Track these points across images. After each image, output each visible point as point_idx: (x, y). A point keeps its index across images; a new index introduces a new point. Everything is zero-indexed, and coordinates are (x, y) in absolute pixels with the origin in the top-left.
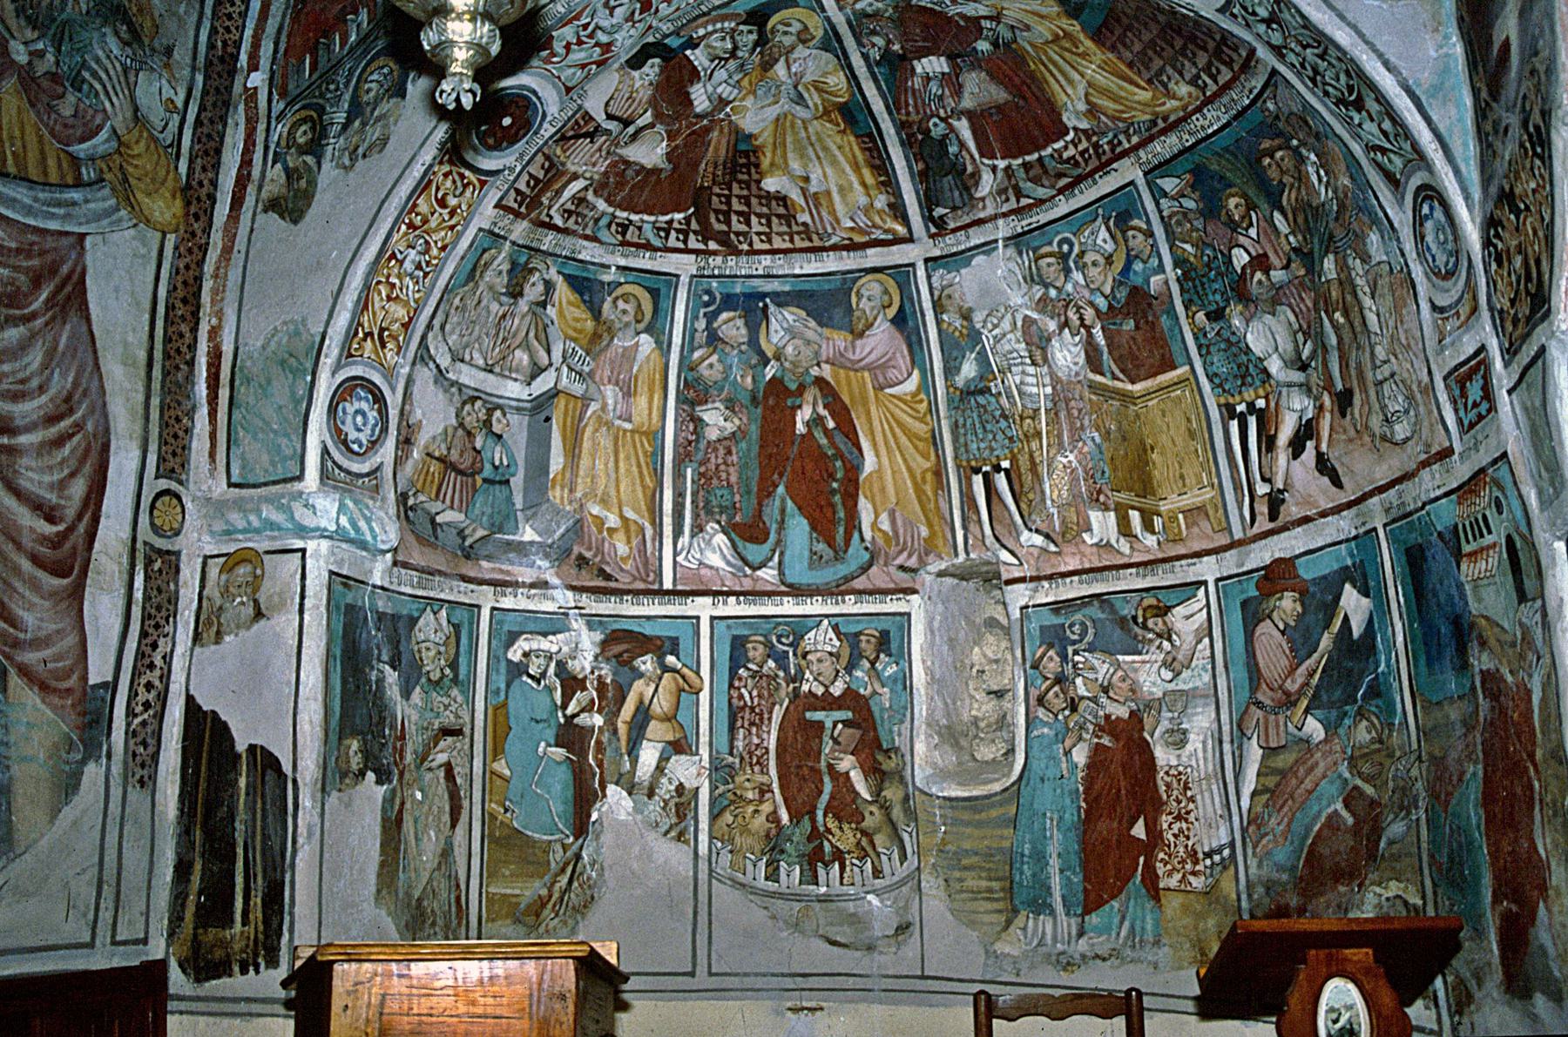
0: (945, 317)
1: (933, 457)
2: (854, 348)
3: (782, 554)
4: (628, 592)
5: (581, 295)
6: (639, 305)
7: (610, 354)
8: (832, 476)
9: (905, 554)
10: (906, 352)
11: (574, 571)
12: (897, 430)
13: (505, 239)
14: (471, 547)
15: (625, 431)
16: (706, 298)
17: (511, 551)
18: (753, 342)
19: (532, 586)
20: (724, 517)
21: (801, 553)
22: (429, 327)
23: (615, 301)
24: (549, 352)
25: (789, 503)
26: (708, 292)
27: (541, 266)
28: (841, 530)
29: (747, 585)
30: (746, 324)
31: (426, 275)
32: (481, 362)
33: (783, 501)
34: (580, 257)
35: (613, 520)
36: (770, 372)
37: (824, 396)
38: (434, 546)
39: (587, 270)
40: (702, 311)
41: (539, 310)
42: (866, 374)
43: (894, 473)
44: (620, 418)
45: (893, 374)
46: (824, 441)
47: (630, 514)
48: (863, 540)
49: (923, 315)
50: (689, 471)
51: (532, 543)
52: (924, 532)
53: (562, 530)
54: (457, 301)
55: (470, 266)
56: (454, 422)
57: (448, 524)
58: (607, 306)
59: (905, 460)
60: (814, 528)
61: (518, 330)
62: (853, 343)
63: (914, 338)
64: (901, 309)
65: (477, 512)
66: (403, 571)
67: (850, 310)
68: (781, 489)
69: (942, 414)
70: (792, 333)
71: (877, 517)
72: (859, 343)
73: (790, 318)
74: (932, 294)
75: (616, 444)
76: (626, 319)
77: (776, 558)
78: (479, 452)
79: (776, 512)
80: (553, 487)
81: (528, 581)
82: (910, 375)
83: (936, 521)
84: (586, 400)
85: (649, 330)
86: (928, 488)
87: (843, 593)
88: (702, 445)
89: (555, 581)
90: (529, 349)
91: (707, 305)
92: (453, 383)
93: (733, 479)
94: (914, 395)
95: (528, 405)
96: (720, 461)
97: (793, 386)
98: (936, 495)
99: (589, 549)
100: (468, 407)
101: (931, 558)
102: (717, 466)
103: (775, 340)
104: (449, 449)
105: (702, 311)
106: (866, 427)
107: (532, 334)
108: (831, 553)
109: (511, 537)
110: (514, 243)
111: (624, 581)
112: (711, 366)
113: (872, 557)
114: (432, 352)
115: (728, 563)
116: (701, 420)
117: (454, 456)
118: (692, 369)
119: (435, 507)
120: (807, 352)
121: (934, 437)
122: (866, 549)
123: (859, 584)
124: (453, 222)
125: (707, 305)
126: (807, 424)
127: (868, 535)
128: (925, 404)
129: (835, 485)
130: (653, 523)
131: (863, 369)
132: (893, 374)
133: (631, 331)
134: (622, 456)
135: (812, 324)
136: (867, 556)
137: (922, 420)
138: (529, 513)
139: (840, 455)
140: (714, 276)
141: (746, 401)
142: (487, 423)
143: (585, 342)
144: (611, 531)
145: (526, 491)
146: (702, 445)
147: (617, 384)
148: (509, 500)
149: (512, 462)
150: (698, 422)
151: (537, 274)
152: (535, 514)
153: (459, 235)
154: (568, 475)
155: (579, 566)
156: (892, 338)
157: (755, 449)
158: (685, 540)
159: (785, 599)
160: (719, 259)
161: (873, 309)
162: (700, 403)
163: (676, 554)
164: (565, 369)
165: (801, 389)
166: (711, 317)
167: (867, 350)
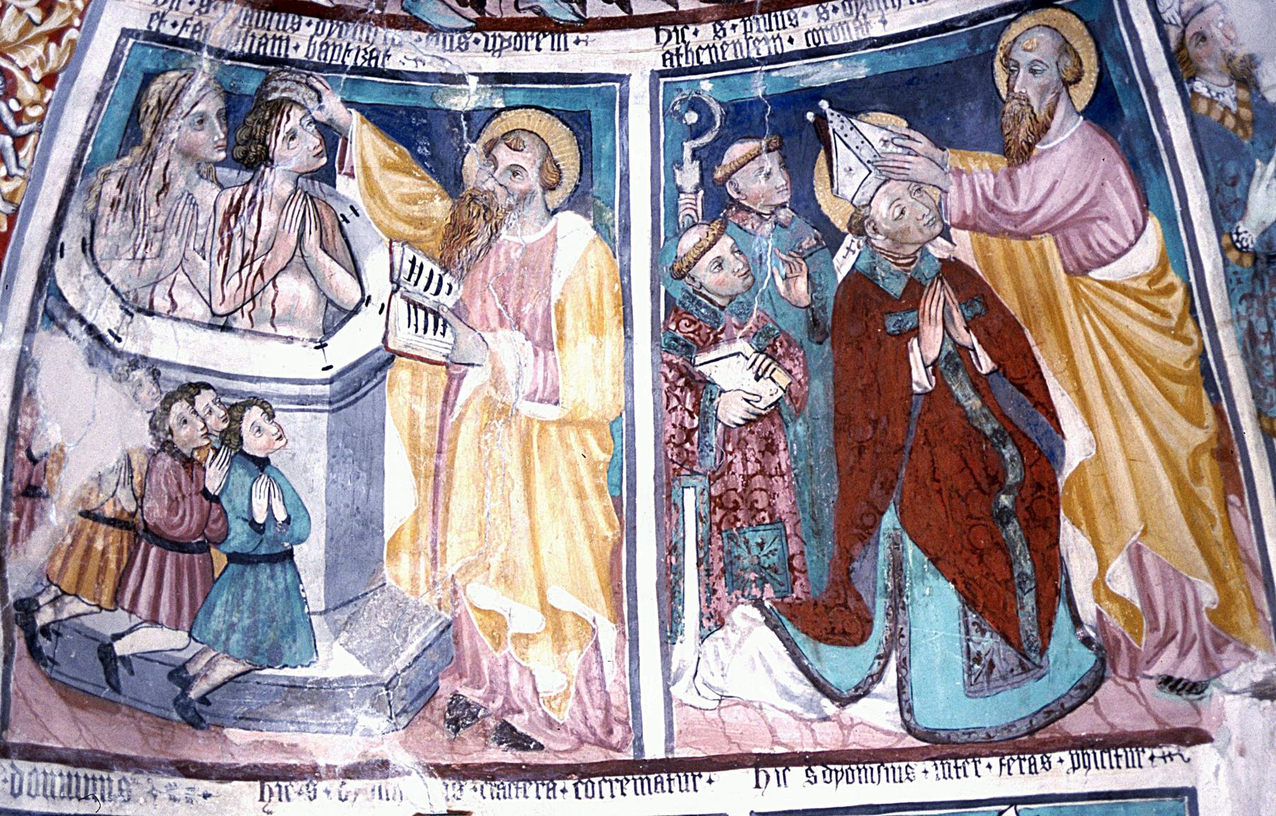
0: (1199, 86)
1: (1209, 418)
2: (1014, 188)
3: (903, 664)
4: (566, 771)
5: (410, 145)
6: (548, 152)
7: (496, 262)
8: (996, 481)
9: (1172, 649)
10: (1126, 182)
11: (442, 735)
12: (1126, 361)
13: (198, 46)
14: (203, 700)
15: (544, 424)
16: (692, 117)
17: (300, 701)
18: (804, 201)
19: (352, 772)
20: (769, 591)
21: (946, 661)
22: (53, 249)
23: (488, 151)
24: (357, 274)
25: (911, 550)
26: (695, 104)
27: (302, 94)
28: (1029, 601)
29: (828, 738)
30: (785, 164)
31: (19, 141)
32: (199, 310)
33: (896, 544)
34: (391, 65)
35: (526, 618)
36: (843, 262)
37: (965, 302)
38: (110, 707)
39: (414, 91)
40: (688, 147)
41: (318, 188)
42: (1048, 242)
43: (1130, 461)
44: (531, 397)
45: (1103, 235)
46: (973, 403)
47: (560, 598)
48: (1077, 622)
49: (1152, 90)
50: (689, 495)
51: (346, 681)
52: (1208, 595)
53: (412, 649)
54: (110, 189)
55: (121, 114)
56: (148, 441)
57: (146, 657)
58: (473, 163)
59: (1153, 433)
60: (969, 600)
61: (275, 235)
62: (1010, 175)
63: (1140, 147)
64: (1103, 84)
65: (216, 624)
66: (25, 766)
67: (994, 103)
68: (890, 520)
69: (1218, 315)
70: (884, 171)
71: (1103, 565)
72: (1022, 172)
73: (875, 136)
74: (1164, 38)
75: (526, 453)
76: (518, 185)
77: (891, 675)
78: (216, 499)
79: (883, 570)
80: (394, 554)
81: (341, 762)
82: (1139, 232)
83: (1229, 566)
84: (454, 368)
85: (578, 201)
86: (1207, 493)
87: (1045, 748)
88: (713, 439)
89: (401, 758)
90: (309, 271)
91: (696, 132)
92: (136, 362)
93: (783, 505)
94: (1154, 278)
95: (326, 389)
96: (752, 467)
97: (896, 288)
98: (1225, 505)
99: (476, 683)
100: (179, 408)
101: (1229, 656)
102: (748, 478)
103: (848, 192)
104: (139, 499)
105: (688, 147)
106: (1061, 364)
107: (312, 240)
108: (1011, 654)
109: (299, 673)
110: (219, 53)
111: (557, 751)
112: (719, 263)
113: (1102, 661)
114: (73, 300)
115: (787, 694)
116: (707, 382)
117: (155, 511)
118: (680, 275)
119: (107, 624)
120: (919, 210)
121: (1205, 370)
122: (1087, 641)
123: (1080, 723)
124: (54, 23)
125: (696, 132)
126: (934, 367)
127: (1087, 608)
128: (1179, 295)
129: (1005, 500)
130: (617, 617)
131: (1038, 231)
132: (1103, 235)
133: (534, 210)
134: (539, 478)
135: (922, 143)
136: (1088, 659)
137: (1177, 334)
138: (341, 616)
139: (1010, 431)
140: (702, 69)
141: (799, 332)
142: (231, 438)
143: (435, 245)
144: (525, 639)
145: (331, 571)
146: (713, 439)
147: (518, 323)
148: (294, 590)
149: (297, 509)
150: (698, 385)
151: (296, 114)
152: (352, 619)
153: (77, 51)
154: (425, 528)
155: (456, 724)
156: (1090, 154)
157: (825, 439)
158: (684, 650)
159: (918, 767)
160: (706, 31)
161: (1043, 90)
162: (705, 346)
163: (669, 679)
164: (399, 306)
165: (915, 291)
166: (708, 158)
167: (1043, 186)
